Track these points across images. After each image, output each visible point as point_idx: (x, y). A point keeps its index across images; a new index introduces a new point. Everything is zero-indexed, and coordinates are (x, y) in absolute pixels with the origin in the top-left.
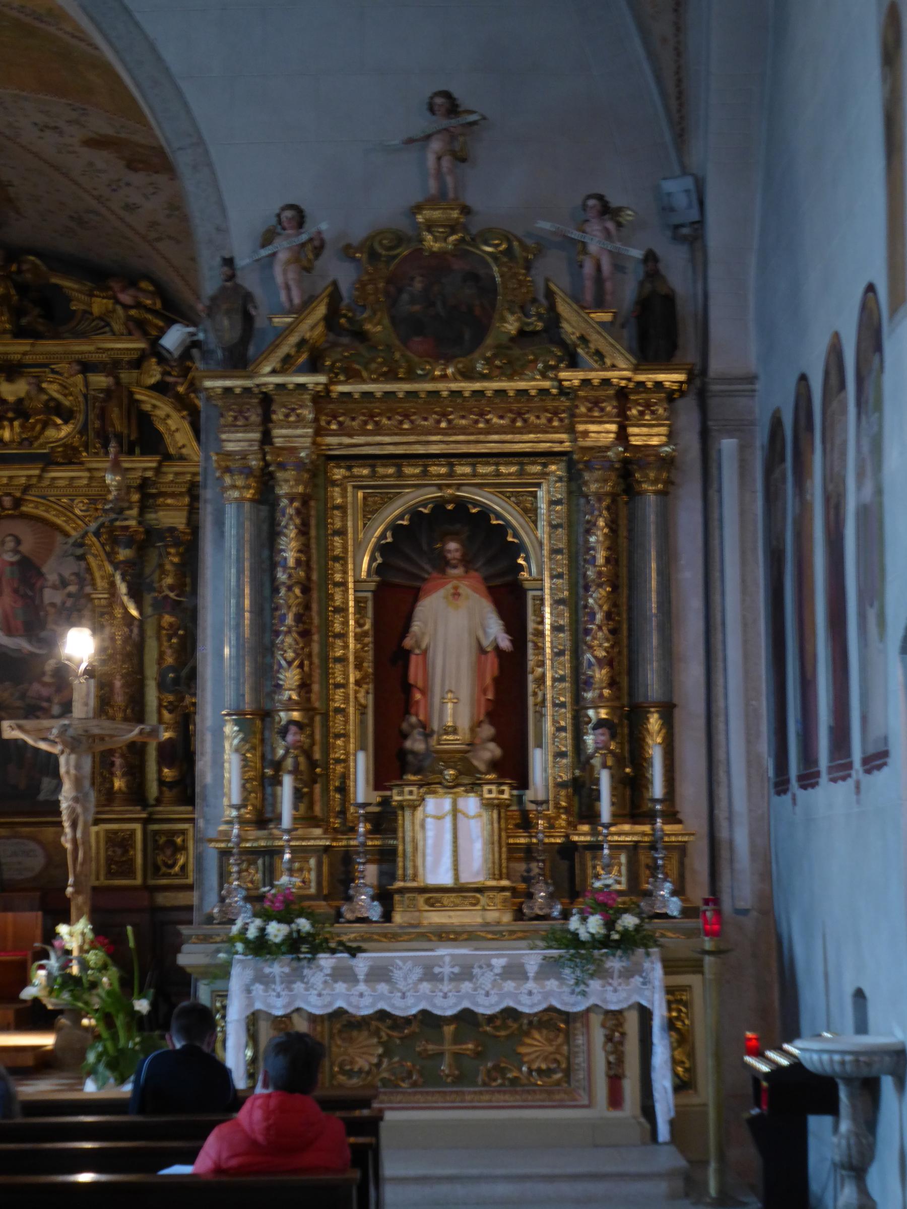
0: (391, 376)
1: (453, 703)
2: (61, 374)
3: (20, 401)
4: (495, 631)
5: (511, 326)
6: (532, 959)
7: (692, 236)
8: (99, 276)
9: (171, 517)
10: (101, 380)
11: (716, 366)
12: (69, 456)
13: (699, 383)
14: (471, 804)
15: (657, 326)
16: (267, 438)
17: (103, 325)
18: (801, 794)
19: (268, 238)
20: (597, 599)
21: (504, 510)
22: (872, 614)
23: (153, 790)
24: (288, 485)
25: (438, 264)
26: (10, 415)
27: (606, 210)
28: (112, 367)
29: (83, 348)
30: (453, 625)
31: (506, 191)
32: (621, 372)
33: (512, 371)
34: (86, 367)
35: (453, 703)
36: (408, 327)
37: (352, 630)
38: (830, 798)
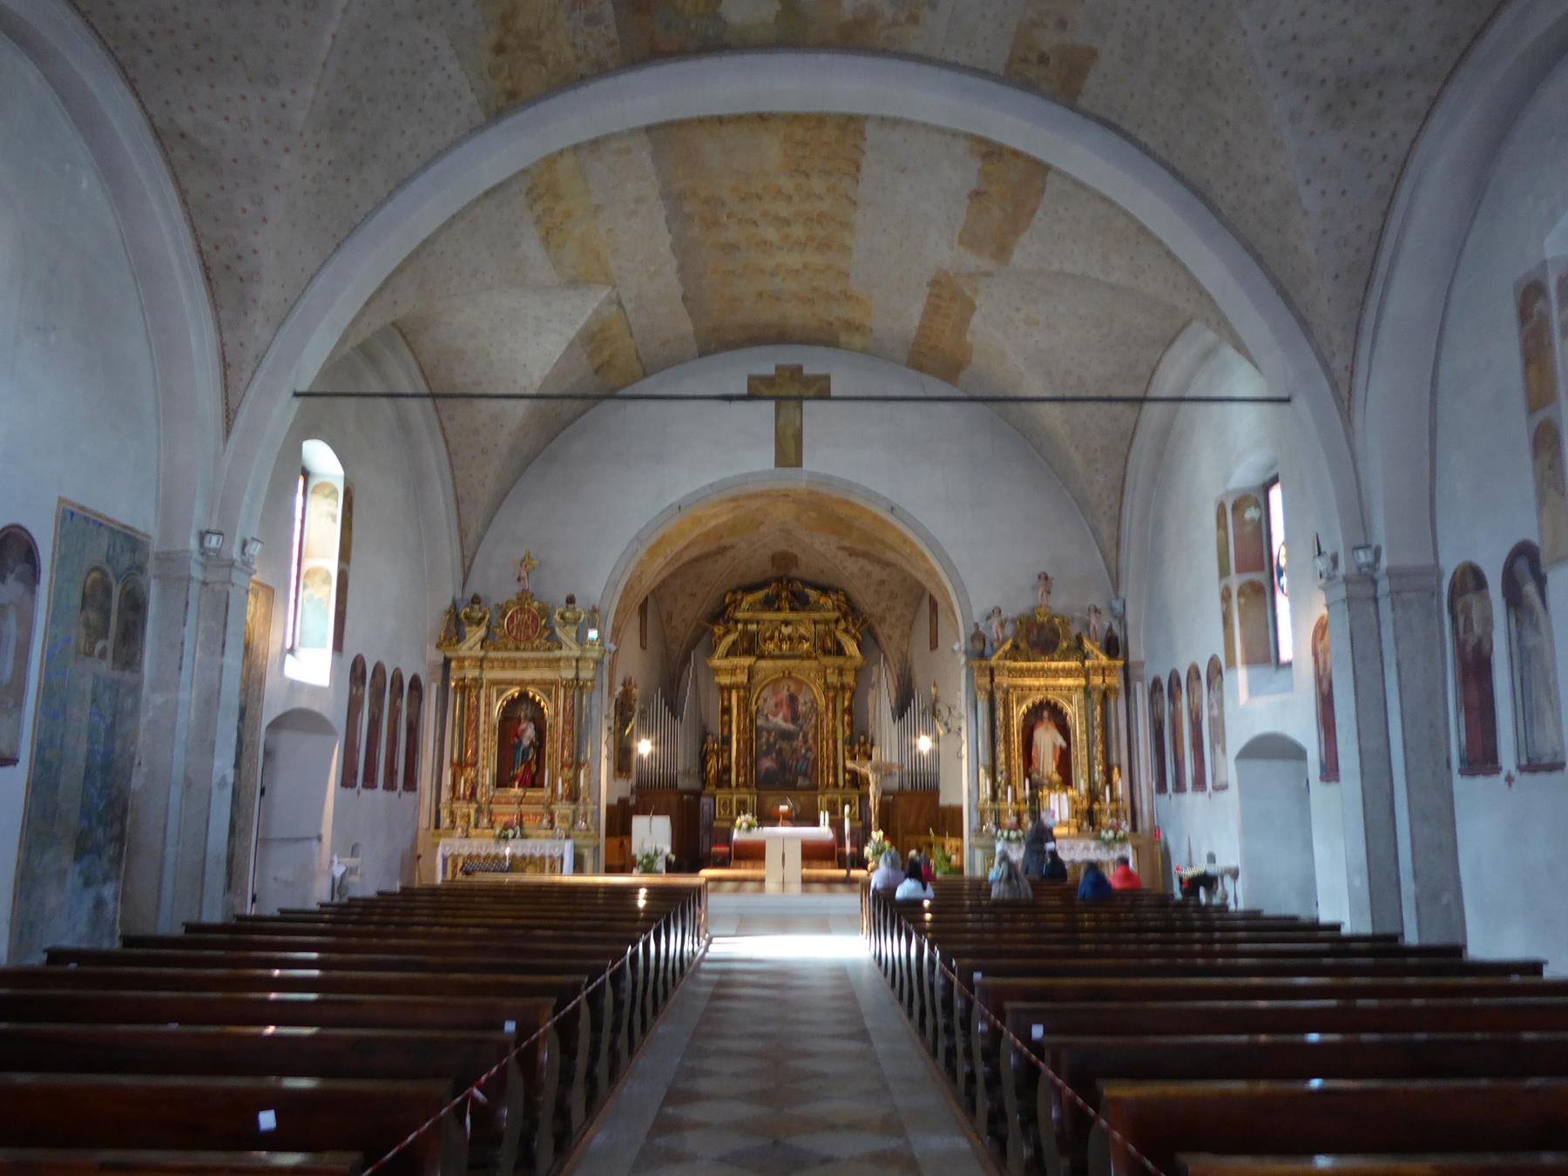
0: (1028, 660)
1: (1047, 763)
4: (1060, 741)
5: (1065, 645)
6: (1092, 844)
7: (1122, 619)
8: (824, 590)
9: (849, 679)
10: (820, 627)
11: (1131, 658)
12: (808, 656)
13: (1126, 668)
14: (1064, 796)
15: (1113, 646)
16: (992, 680)
17: (818, 608)
18: (1174, 797)
19: (988, 618)
20: (1098, 732)
21: (1062, 703)
22: (1219, 750)
23: (841, 783)
24: (999, 696)
25: (1042, 626)
27: (1096, 610)
28: (827, 622)
29: (816, 616)
30: (1047, 739)
31: (1059, 602)
32: (1104, 660)
33: (1066, 659)
34: (815, 622)
35: (1047, 763)
36: (1033, 645)
37: (1016, 740)
38: (1191, 798)
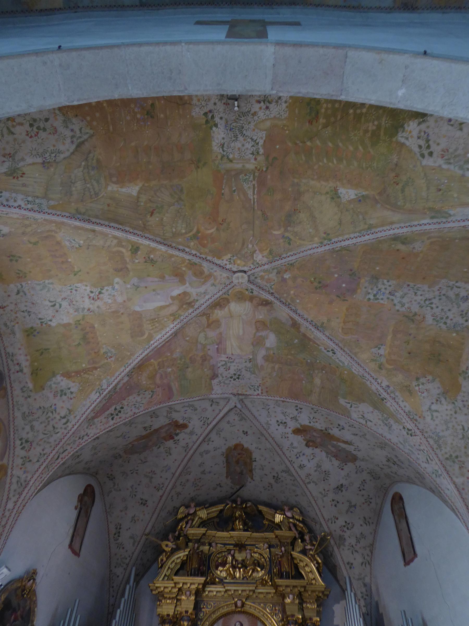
2: (260, 549)
3: (243, 561)
26: (240, 566)
29: (270, 535)
